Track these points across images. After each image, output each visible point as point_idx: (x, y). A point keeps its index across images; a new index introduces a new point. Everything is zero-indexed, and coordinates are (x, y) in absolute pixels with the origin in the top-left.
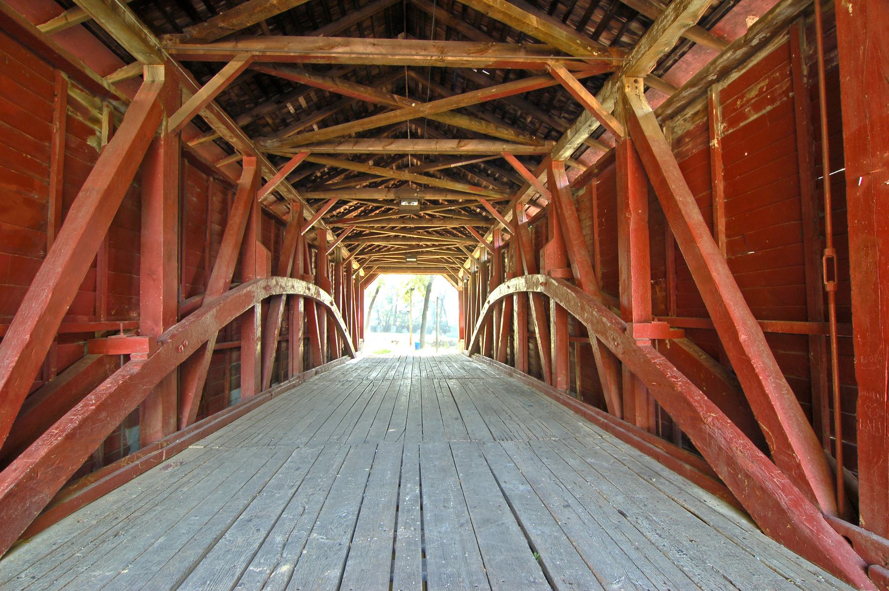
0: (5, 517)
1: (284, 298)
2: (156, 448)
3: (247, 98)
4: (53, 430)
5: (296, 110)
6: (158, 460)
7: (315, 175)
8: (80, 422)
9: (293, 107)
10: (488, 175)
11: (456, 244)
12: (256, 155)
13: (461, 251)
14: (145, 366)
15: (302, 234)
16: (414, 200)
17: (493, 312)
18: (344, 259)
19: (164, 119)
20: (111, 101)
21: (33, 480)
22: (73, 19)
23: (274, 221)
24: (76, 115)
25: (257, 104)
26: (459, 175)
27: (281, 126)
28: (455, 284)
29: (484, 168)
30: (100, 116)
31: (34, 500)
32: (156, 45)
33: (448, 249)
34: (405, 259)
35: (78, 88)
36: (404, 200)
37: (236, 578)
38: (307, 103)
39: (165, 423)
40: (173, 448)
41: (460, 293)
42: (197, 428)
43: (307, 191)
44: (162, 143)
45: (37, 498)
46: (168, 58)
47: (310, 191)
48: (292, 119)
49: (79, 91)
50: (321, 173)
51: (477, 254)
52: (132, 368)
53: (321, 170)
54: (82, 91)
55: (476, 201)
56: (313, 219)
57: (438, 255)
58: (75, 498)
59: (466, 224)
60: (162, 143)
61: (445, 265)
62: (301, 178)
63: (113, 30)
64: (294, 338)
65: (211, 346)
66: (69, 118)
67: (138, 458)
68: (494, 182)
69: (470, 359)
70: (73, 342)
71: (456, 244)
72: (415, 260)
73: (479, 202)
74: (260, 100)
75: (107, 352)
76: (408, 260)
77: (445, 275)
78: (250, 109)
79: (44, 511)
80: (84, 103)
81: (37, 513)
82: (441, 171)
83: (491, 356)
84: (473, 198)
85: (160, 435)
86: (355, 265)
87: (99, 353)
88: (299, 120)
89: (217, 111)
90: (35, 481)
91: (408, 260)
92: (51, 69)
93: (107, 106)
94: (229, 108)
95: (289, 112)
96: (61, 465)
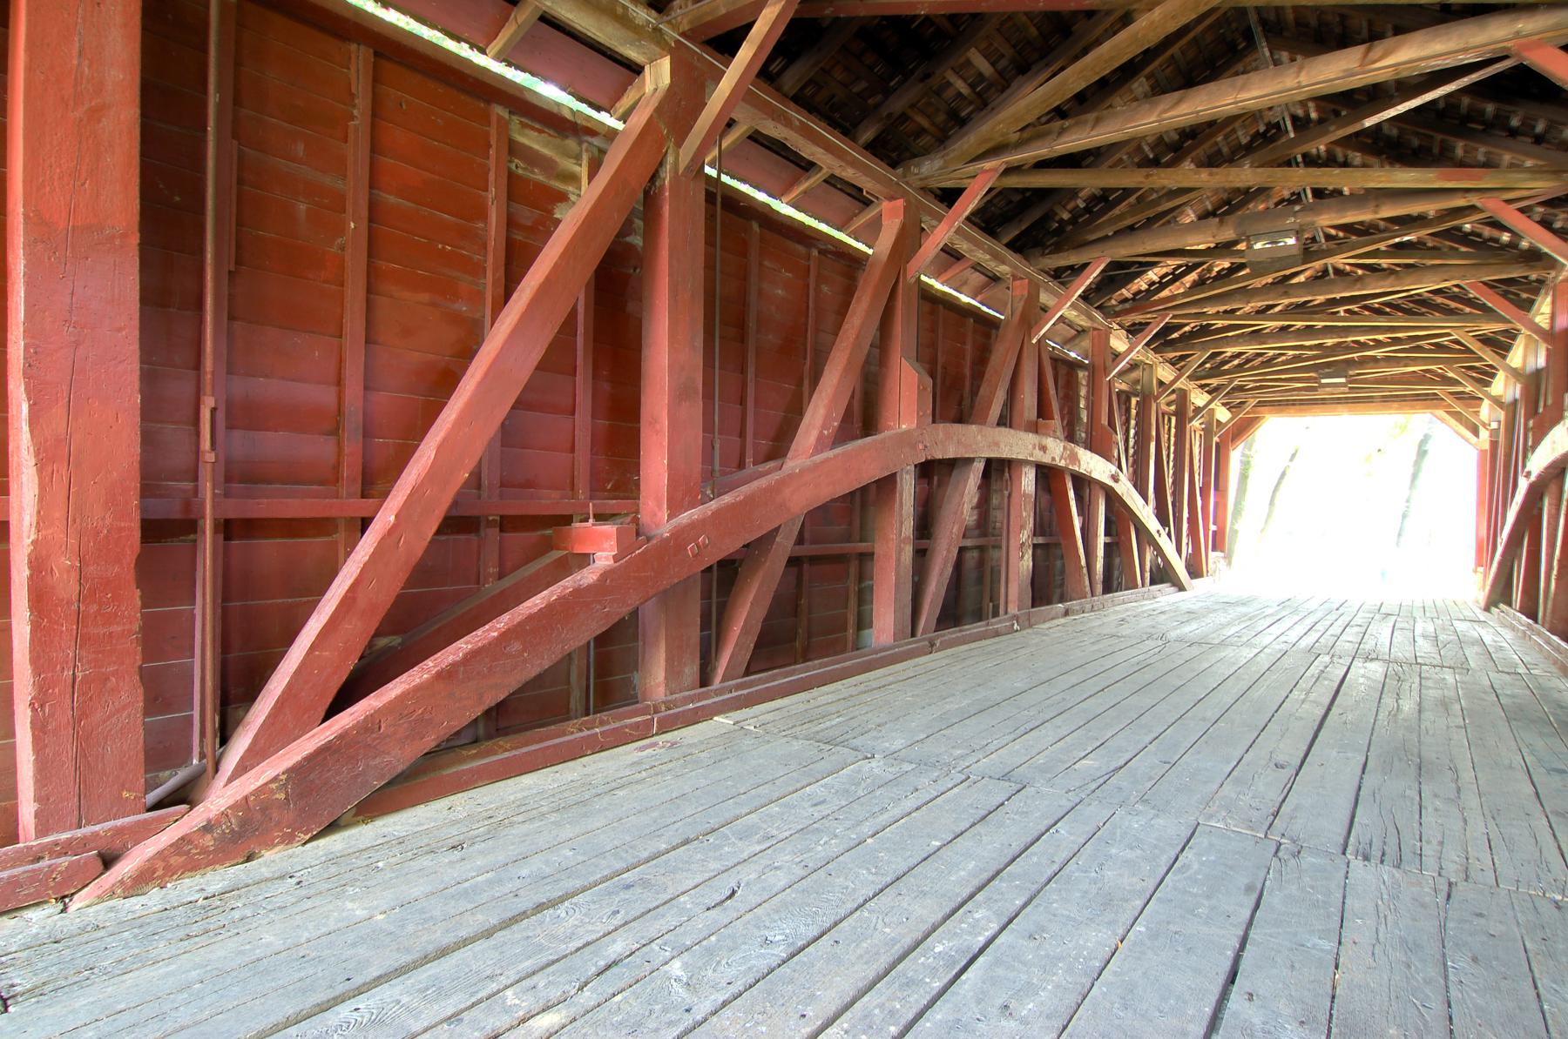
0: (317, 782)
1: (979, 466)
2: (645, 711)
3: (862, 85)
4: (429, 663)
5: (972, 86)
6: (642, 732)
7: (1057, 218)
8: (466, 655)
9: (965, 80)
10: (1513, 133)
11: (1449, 335)
12: (905, 194)
13: (1468, 351)
14: (606, 575)
15: (1034, 341)
16: (1286, 233)
17: (1541, 499)
18: (1161, 383)
19: (670, 151)
20: (589, 139)
21: (372, 733)
22: (524, 17)
23: (972, 320)
24: (533, 172)
25: (888, 93)
26: (1429, 150)
27: (951, 129)
28: (1469, 435)
29: (1496, 116)
30: (577, 168)
31: (372, 763)
32: (650, 22)
33: (1439, 347)
34: (1315, 380)
35: (533, 129)
36: (1258, 237)
37: (474, 1000)
38: (993, 64)
39: (673, 672)
40: (677, 715)
41: (1482, 452)
42: (739, 687)
43: (1043, 255)
44: (667, 194)
45: (378, 761)
46: (677, 42)
47: (1049, 253)
48: (971, 108)
49: (536, 134)
50: (1070, 212)
51: (1516, 358)
52: (587, 577)
53: (1071, 206)
54: (540, 131)
55: (1472, 209)
56: (1066, 307)
57: (1406, 366)
58: (463, 770)
59: (1463, 277)
60: (667, 194)
61: (1437, 389)
62: (1023, 228)
63: (570, 16)
64: (1012, 542)
65: (785, 546)
66: (511, 176)
67: (602, 723)
68: (1536, 149)
69: (1482, 616)
70: (535, 529)
71: (1451, 335)
72: (1343, 380)
73: (1481, 211)
74: (892, 84)
75: (572, 548)
76: (1323, 381)
77: (1441, 413)
78: (877, 106)
79: (389, 783)
80: (546, 151)
81: (378, 784)
82: (1346, 142)
83: (1533, 616)
84: (1460, 202)
85: (662, 689)
86: (1199, 398)
87: (565, 549)
88: (986, 105)
89: (801, 121)
90: (374, 735)
91: (1323, 381)
92: (482, 105)
93: (587, 151)
94: (837, 115)
95: (960, 94)
96: (427, 717)
